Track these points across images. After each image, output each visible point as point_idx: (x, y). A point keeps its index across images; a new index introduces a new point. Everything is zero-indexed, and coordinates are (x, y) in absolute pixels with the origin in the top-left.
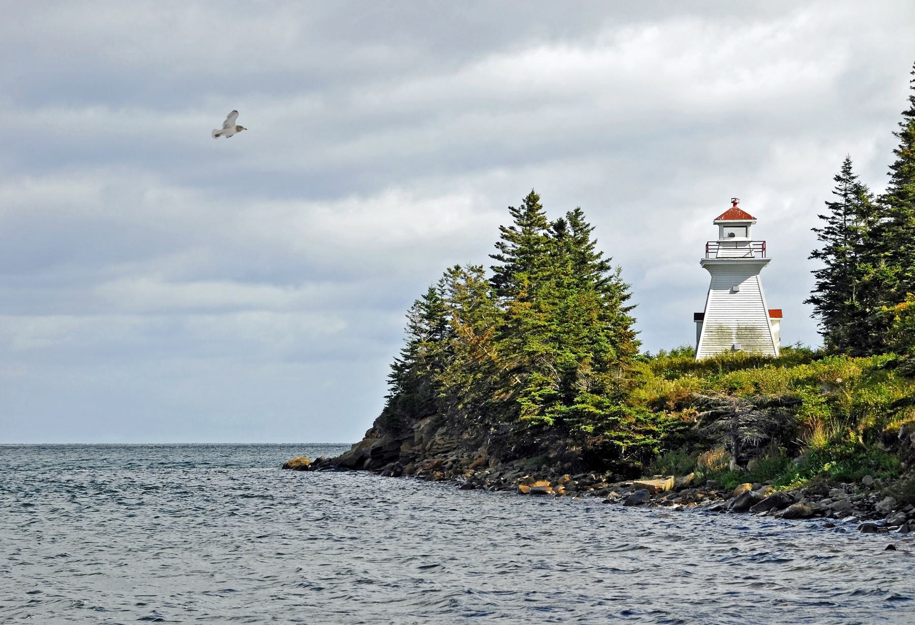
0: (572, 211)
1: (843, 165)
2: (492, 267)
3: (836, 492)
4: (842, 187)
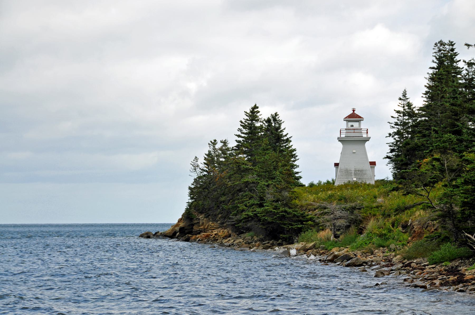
0: (273, 114)
1: (403, 92)
2: (236, 141)
3: (377, 252)
4: (402, 103)
